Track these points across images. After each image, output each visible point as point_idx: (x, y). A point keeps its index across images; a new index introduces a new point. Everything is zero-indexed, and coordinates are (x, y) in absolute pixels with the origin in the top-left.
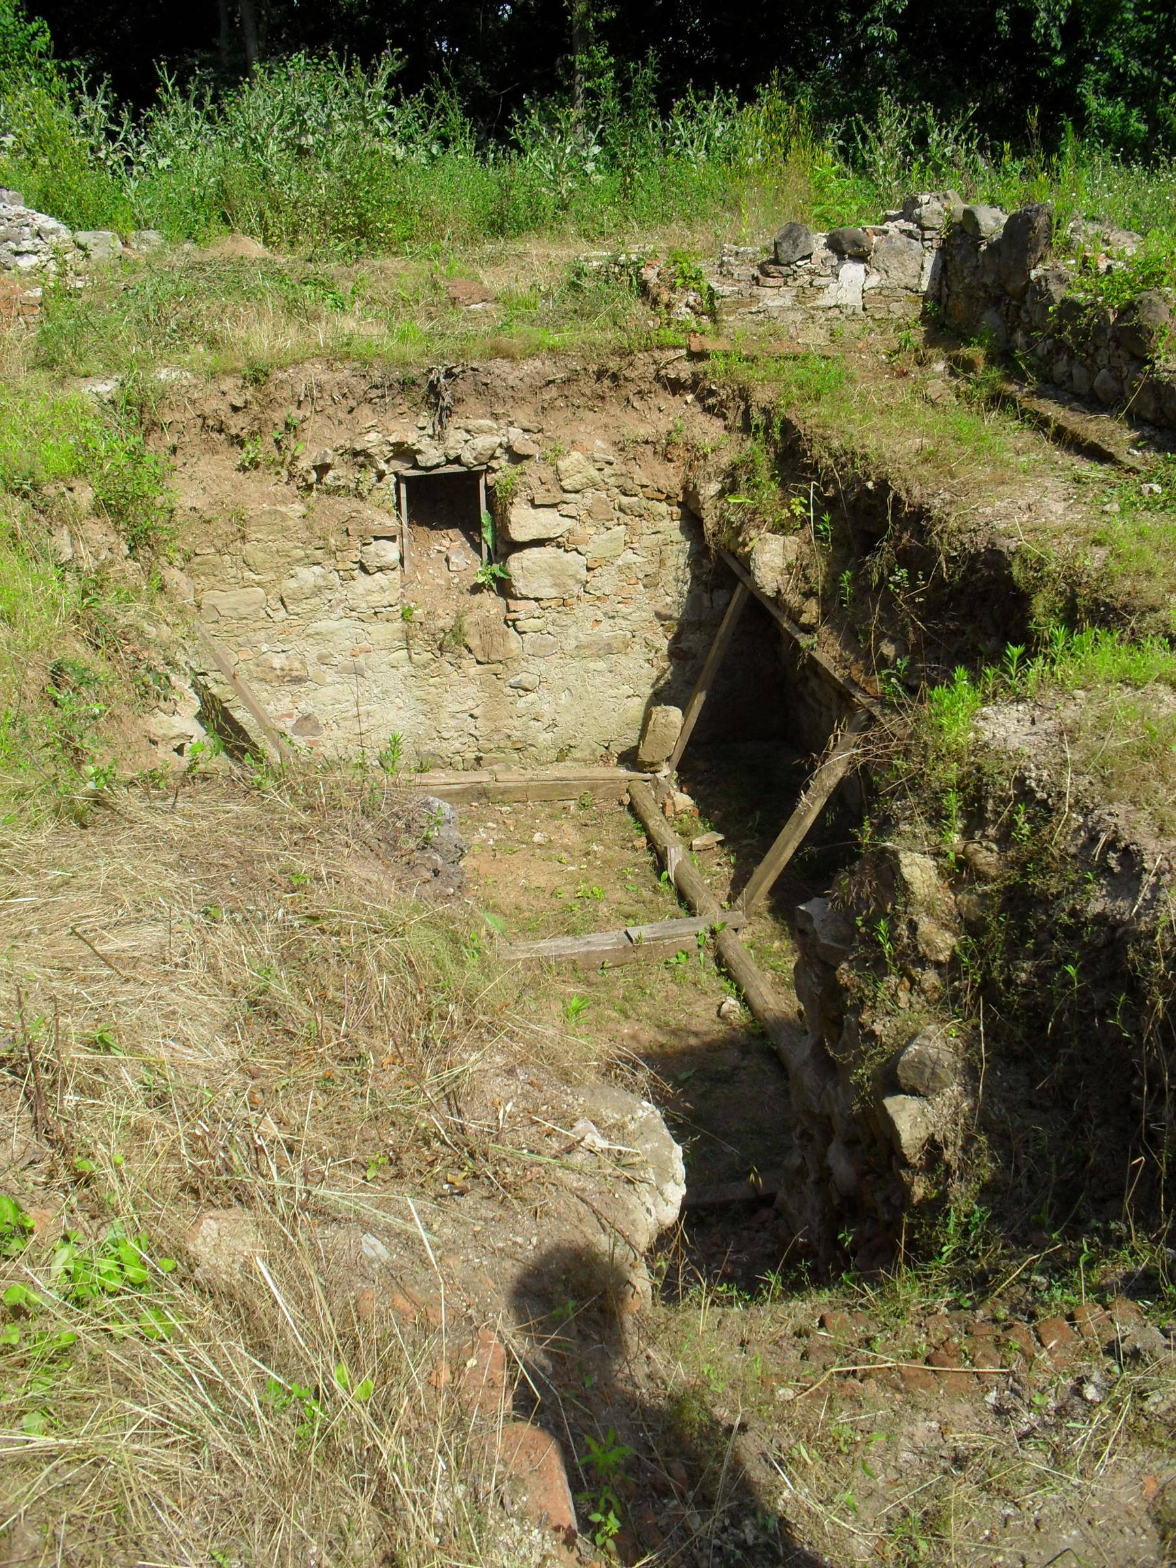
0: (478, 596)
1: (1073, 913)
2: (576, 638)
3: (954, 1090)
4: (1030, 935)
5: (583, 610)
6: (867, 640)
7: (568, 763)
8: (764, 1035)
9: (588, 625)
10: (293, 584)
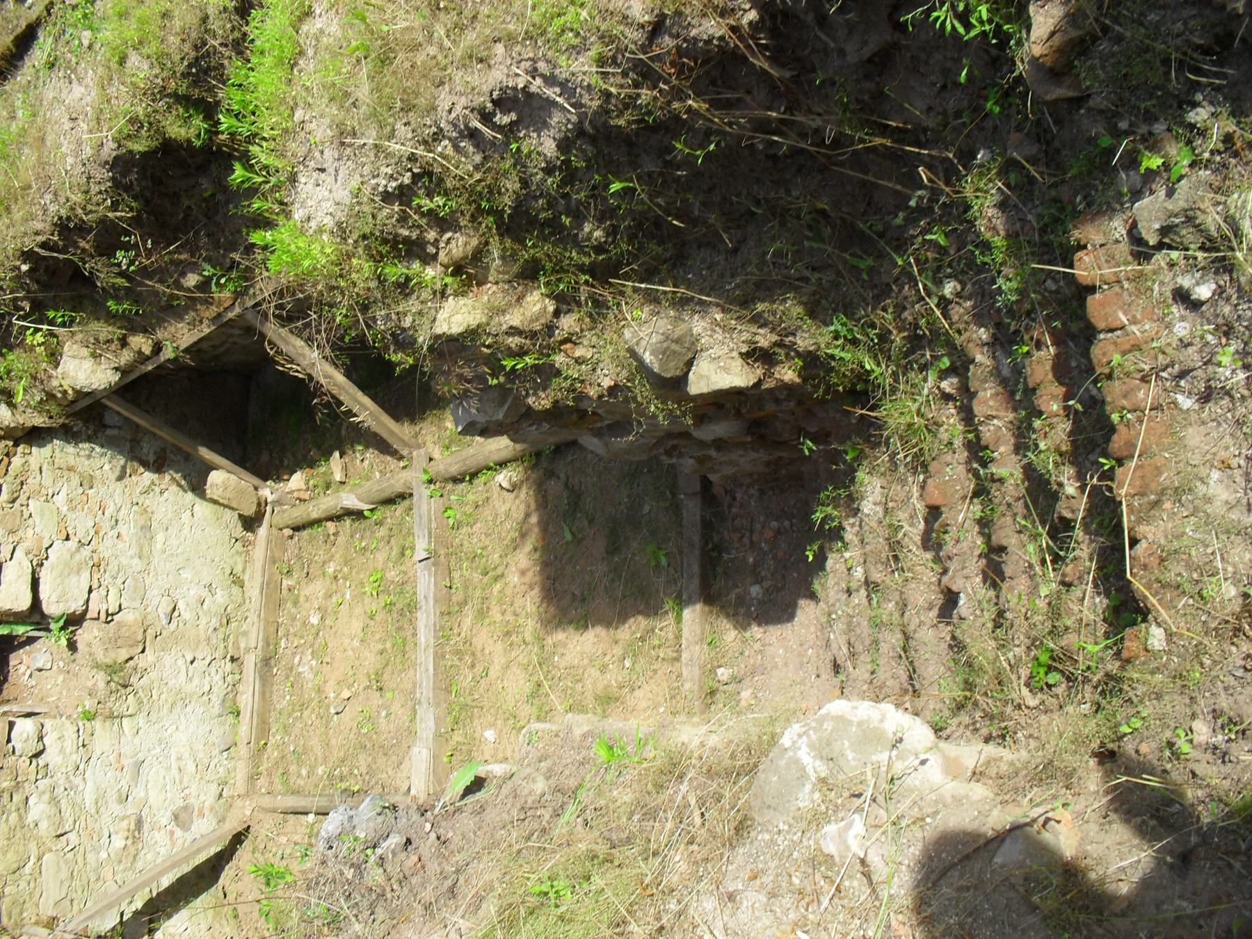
0: (79, 645)
1: (549, 171)
2: (132, 558)
3: (698, 325)
4: (556, 218)
5: (106, 549)
6: (178, 298)
7: (246, 578)
8: (538, 454)
9: (120, 545)
10: (44, 825)
